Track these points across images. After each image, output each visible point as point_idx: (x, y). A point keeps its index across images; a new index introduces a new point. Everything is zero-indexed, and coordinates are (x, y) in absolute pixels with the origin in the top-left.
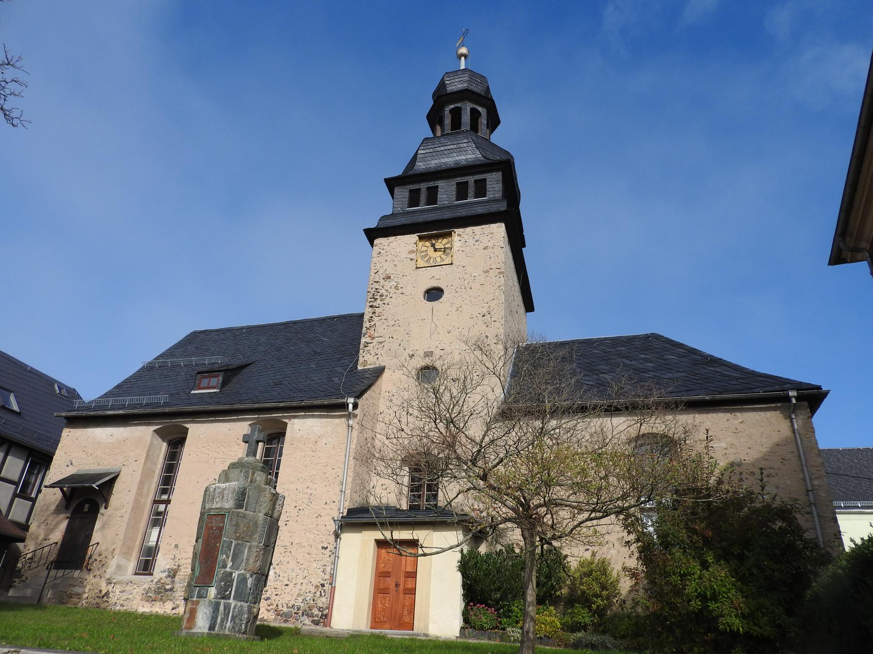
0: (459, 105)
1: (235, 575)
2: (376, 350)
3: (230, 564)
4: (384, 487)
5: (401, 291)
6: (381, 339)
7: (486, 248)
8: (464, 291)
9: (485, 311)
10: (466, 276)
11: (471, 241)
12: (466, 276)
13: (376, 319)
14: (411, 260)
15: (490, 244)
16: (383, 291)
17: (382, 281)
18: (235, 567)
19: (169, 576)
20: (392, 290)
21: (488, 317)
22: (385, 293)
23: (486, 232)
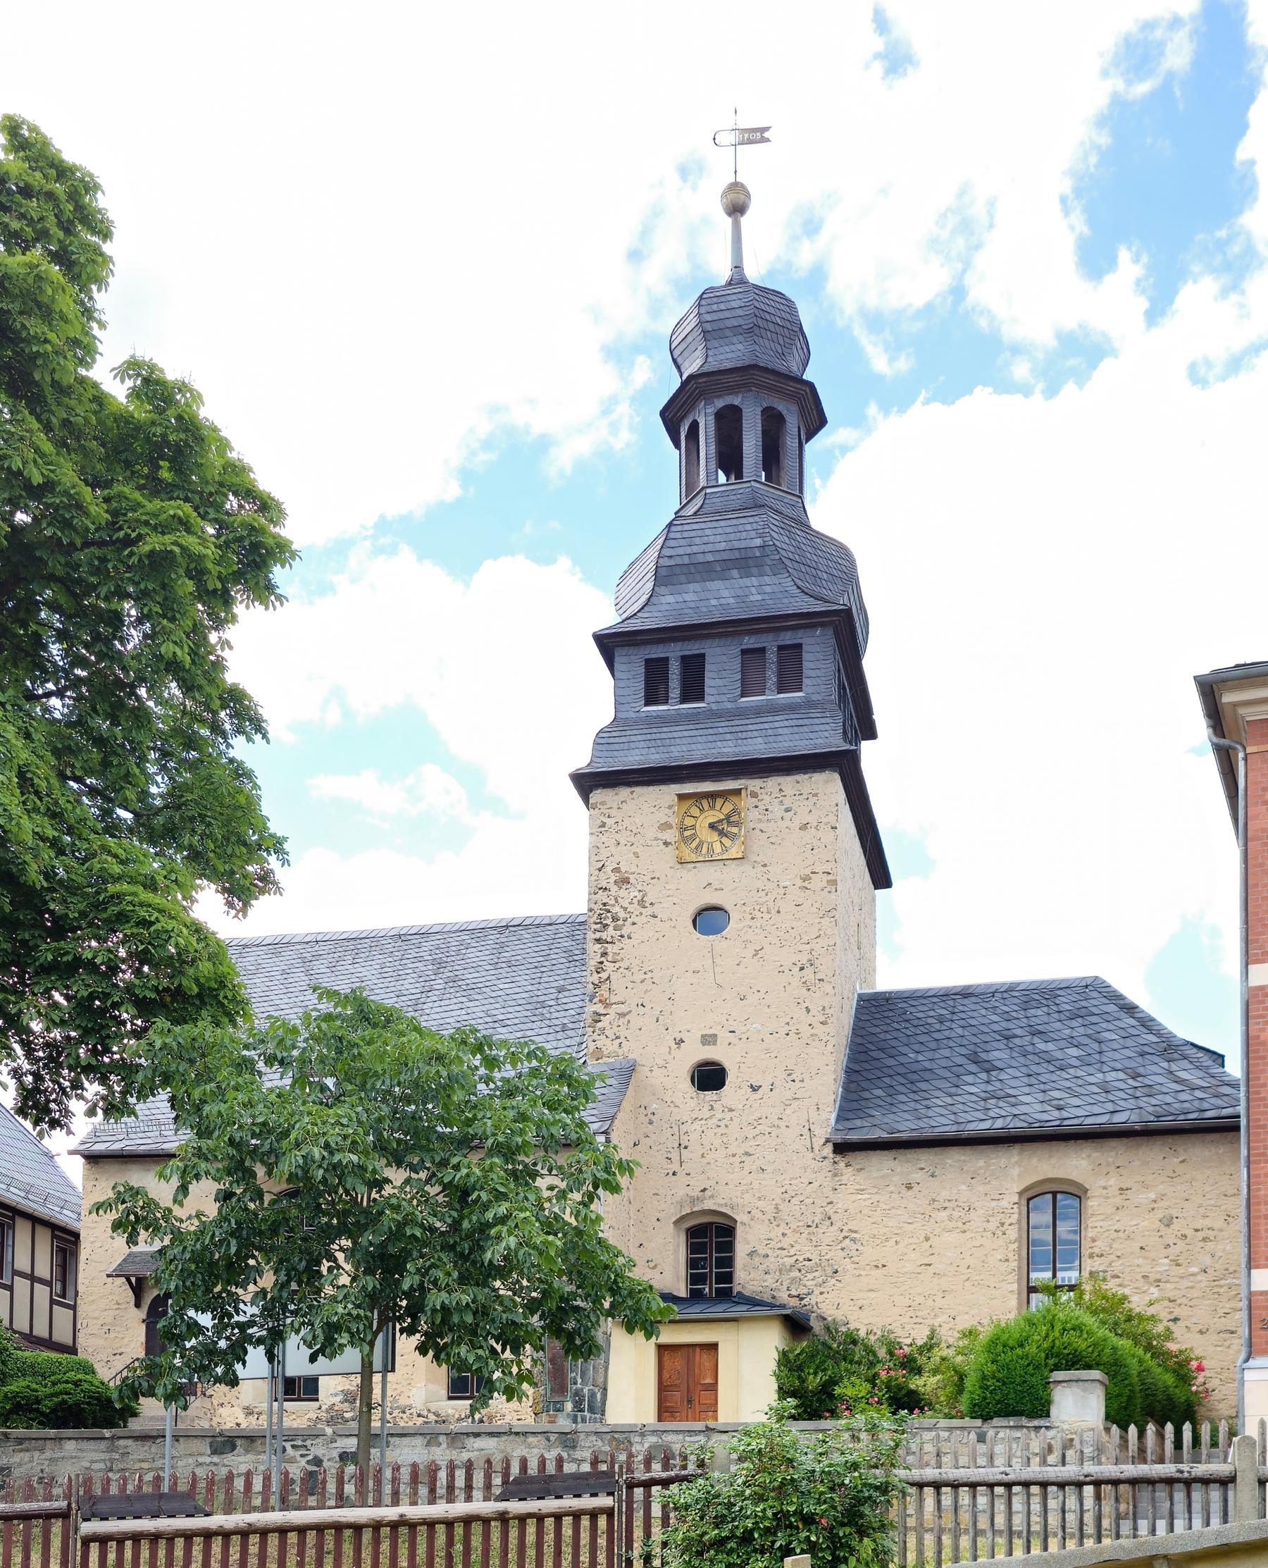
0: (736, 401)
1: (586, 1391)
2: (615, 1029)
3: (579, 1381)
4: (651, 1264)
5: (649, 910)
6: (622, 1009)
7: (804, 827)
8: (767, 916)
9: (804, 959)
10: (770, 886)
11: (777, 810)
12: (770, 886)
13: (609, 967)
14: (666, 844)
15: (812, 819)
16: (616, 909)
17: (614, 888)
18: (584, 1383)
19: (346, 1401)
20: (634, 908)
21: (808, 972)
22: (622, 915)
23: (805, 791)
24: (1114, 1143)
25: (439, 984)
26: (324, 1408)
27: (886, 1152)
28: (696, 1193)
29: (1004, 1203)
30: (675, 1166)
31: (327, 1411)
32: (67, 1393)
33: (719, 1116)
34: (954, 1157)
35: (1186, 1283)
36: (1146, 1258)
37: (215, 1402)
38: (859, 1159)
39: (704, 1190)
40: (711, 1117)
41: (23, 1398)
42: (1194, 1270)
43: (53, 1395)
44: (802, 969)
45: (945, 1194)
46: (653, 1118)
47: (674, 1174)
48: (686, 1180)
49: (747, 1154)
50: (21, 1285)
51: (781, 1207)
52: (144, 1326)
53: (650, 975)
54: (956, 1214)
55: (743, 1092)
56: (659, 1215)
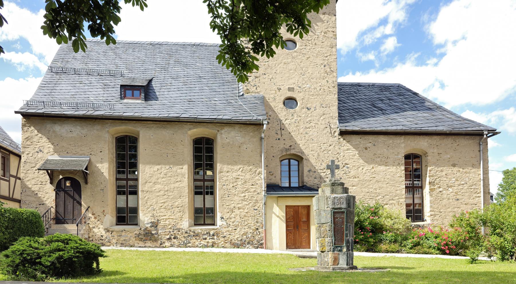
4: (271, 174)
24: (435, 137)
25: (172, 62)
26: (142, 229)
27: (357, 136)
28: (288, 147)
29: (400, 156)
30: (279, 137)
31: (144, 230)
32: (59, 250)
33: (295, 118)
34: (382, 138)
35: (461, 187)
36: (447, 178)
37: (91, 226)
38: (348, 137)
39: (291, 146)
40: (292, 119)
41: (28, 255)
42: (463, 183)
43: (51, 252)
44: (325, 66)
45: (379, 152)
46: (270, 118)
47: (279, 139)
48: (284, 142)
49: (306, 133)
50: (12, 180)
51: (320, 154)
52: (55, 192)
53: (267, 63)
54: (383, 159)
55: (304, 110)
56: (273, 155)
